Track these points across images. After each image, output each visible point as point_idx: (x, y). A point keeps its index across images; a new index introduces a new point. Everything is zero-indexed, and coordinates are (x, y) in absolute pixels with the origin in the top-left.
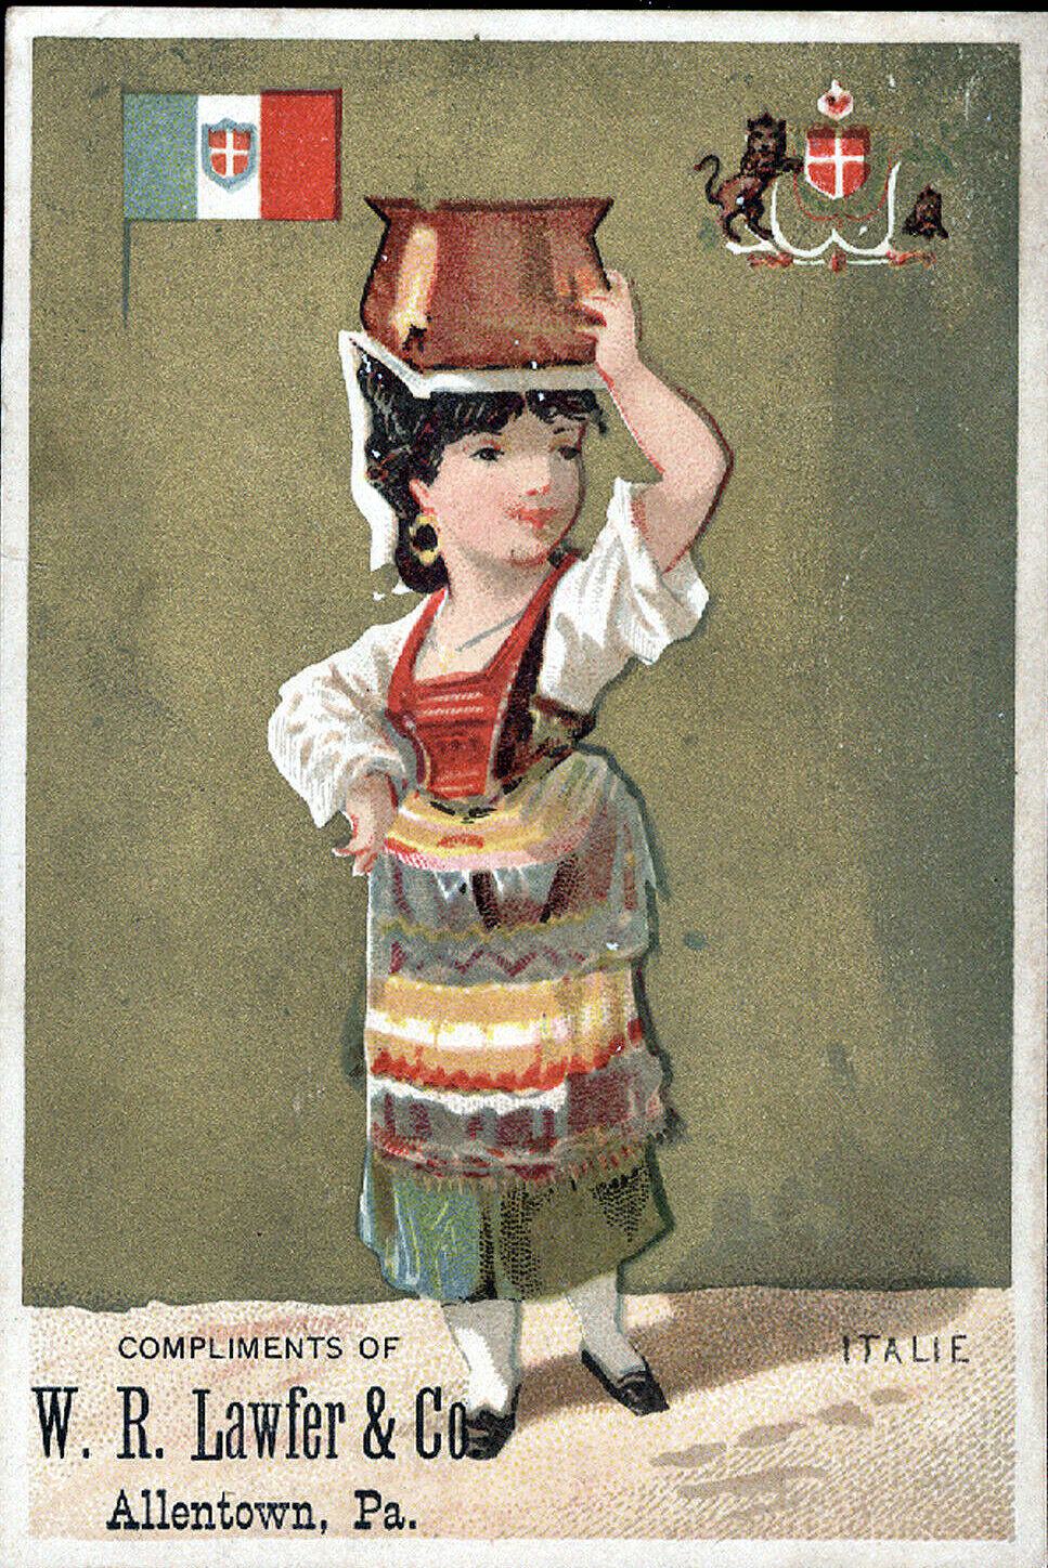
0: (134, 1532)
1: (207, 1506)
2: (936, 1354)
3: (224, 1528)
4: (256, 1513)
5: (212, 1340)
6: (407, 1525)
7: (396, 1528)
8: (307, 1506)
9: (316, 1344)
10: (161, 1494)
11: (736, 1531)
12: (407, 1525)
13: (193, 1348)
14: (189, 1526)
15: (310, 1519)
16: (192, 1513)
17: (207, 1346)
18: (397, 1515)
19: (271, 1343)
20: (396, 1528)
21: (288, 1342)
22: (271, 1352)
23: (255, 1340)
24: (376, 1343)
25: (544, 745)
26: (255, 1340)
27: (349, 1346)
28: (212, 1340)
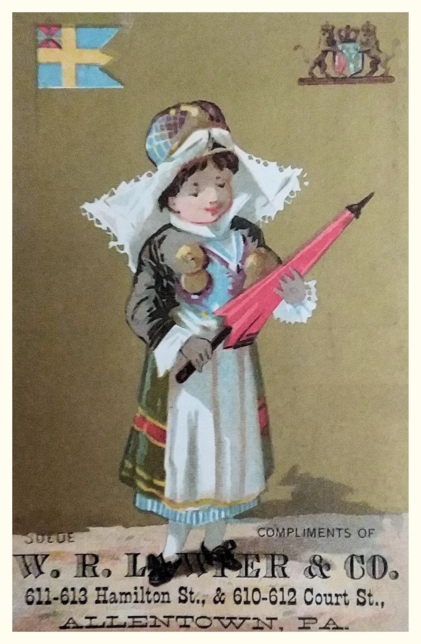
0: (164, 604)
1: (327, 604)
2: (334, 531)
3: (148, 602)
4: (324, 598)
5: (296, 529)
6: (374, 604)
7: (220, 603)
8: (167, 593)
9: (339, 531)
10: (142, 588)
11: (393, 608)
12: (374, 604)
13: (288, 533)
14: (242, 602)
15: (169, 598)
16: (162, 596)
17: (294, 532)
18: (115, 598)
19: (322, 530)
20: (220, 603)
21: (328, 530)
22: (321, 534)
23: (283, 529)
24: (365, 531)
25: (150, 245)
26: (314, 530)
27: (354, 532)
28: (296, 529)
